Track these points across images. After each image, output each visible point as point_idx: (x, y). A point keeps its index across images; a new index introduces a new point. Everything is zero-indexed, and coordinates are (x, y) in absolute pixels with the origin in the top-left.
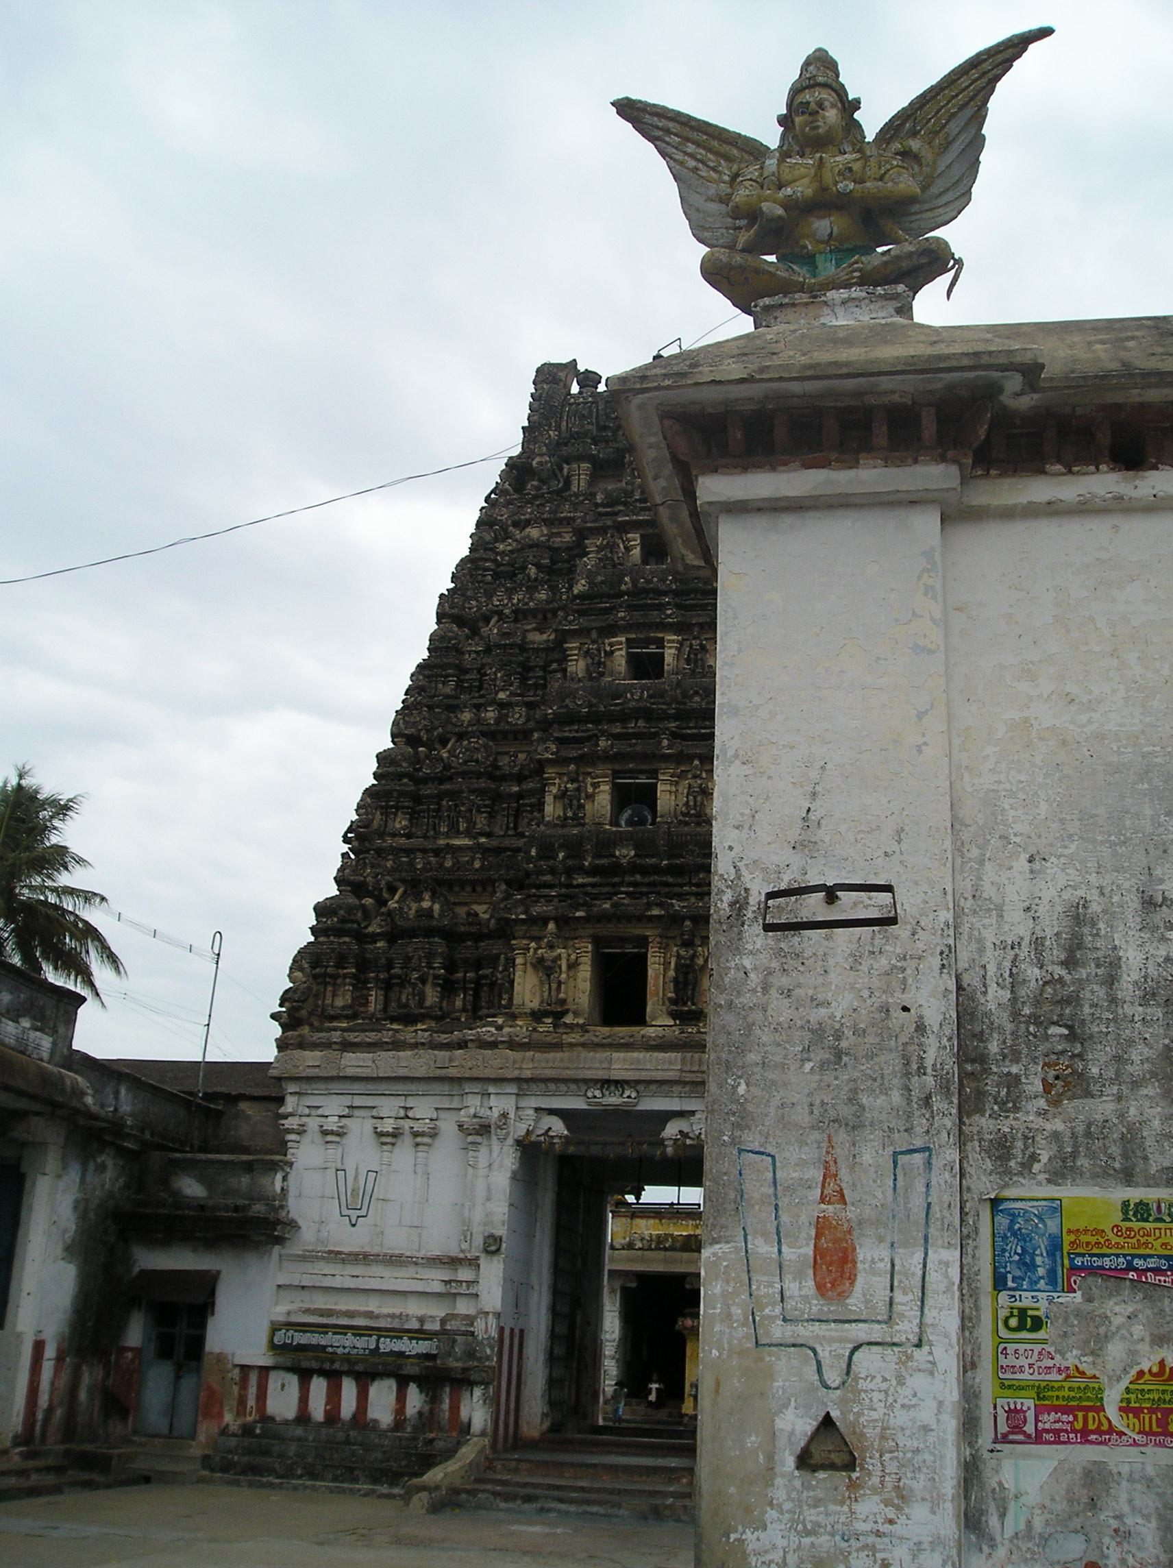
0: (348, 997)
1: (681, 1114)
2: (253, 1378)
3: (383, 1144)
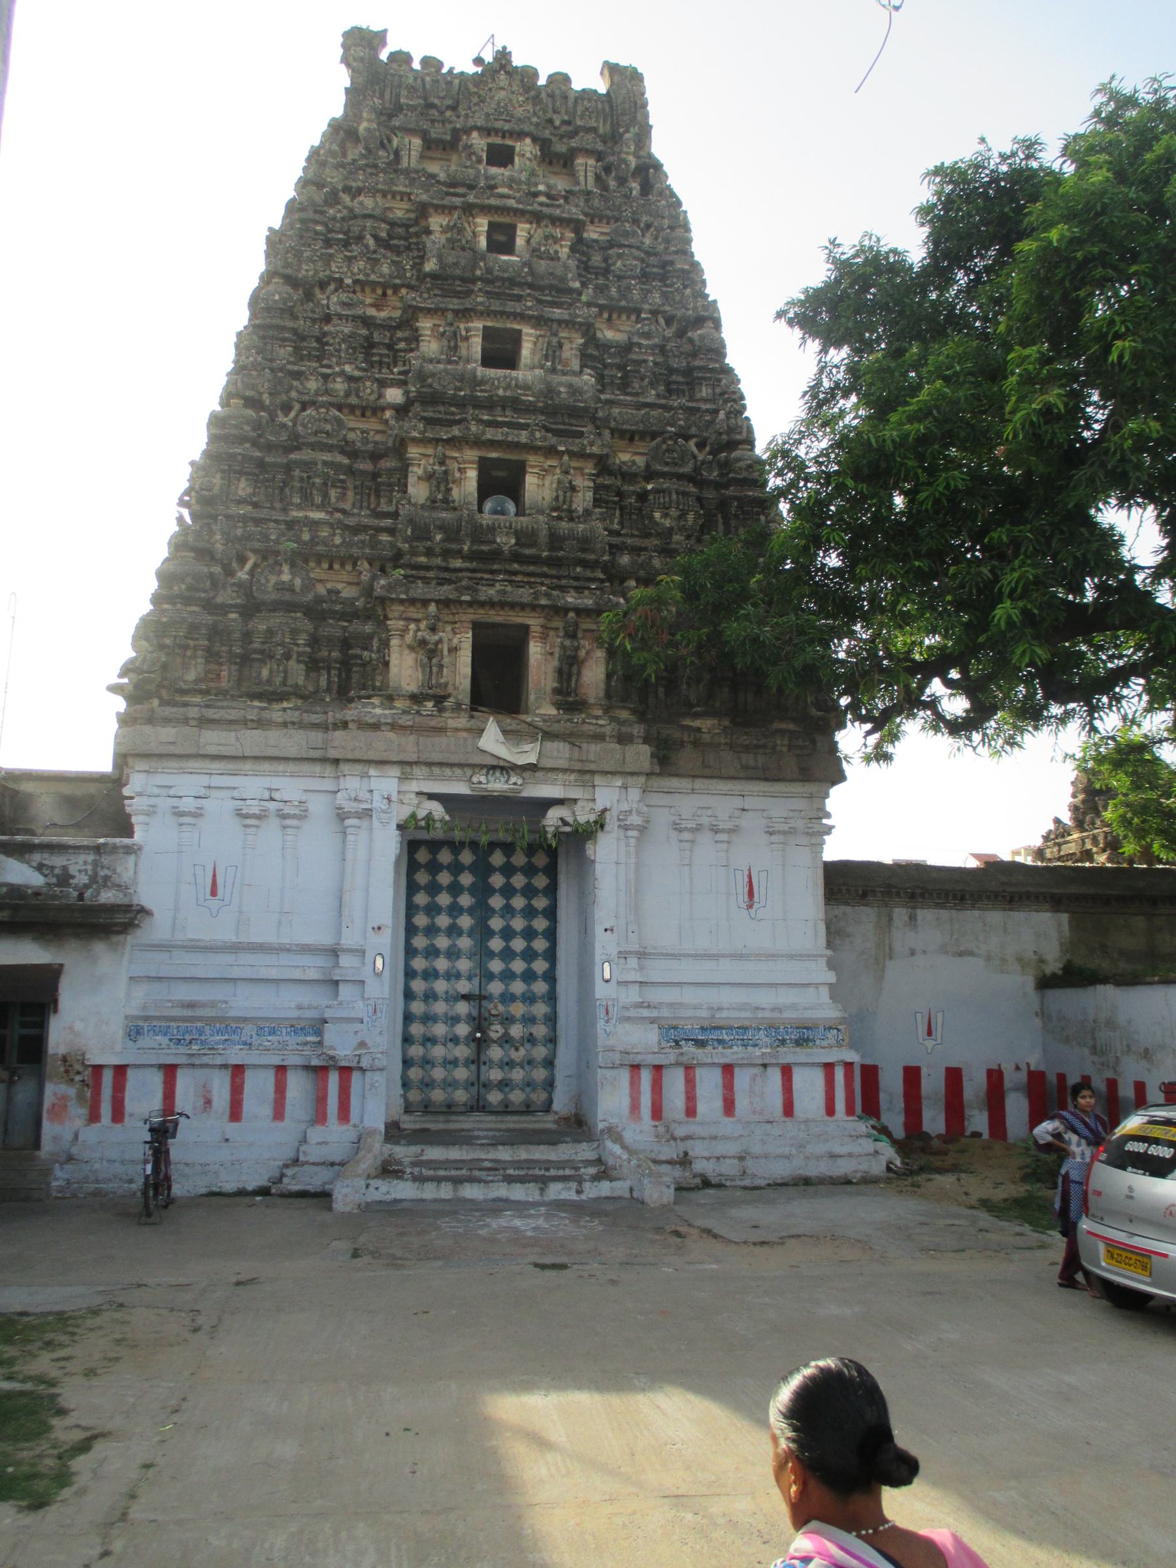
0: (201, 668)
1: (560, 802)
2: (108, 1077)
3: (246, 826)
